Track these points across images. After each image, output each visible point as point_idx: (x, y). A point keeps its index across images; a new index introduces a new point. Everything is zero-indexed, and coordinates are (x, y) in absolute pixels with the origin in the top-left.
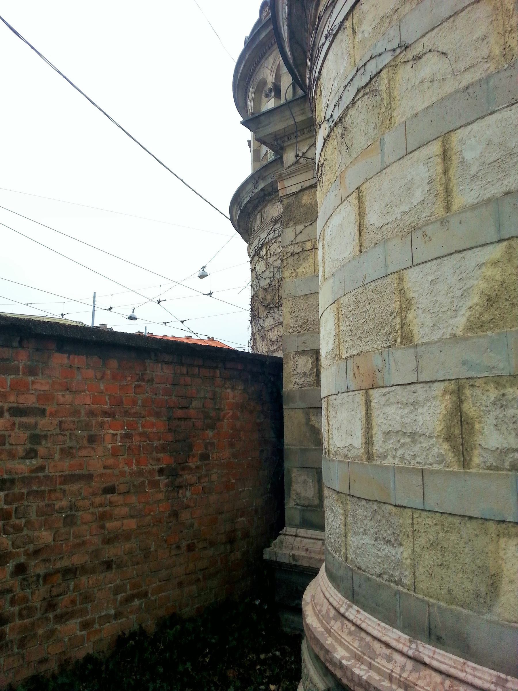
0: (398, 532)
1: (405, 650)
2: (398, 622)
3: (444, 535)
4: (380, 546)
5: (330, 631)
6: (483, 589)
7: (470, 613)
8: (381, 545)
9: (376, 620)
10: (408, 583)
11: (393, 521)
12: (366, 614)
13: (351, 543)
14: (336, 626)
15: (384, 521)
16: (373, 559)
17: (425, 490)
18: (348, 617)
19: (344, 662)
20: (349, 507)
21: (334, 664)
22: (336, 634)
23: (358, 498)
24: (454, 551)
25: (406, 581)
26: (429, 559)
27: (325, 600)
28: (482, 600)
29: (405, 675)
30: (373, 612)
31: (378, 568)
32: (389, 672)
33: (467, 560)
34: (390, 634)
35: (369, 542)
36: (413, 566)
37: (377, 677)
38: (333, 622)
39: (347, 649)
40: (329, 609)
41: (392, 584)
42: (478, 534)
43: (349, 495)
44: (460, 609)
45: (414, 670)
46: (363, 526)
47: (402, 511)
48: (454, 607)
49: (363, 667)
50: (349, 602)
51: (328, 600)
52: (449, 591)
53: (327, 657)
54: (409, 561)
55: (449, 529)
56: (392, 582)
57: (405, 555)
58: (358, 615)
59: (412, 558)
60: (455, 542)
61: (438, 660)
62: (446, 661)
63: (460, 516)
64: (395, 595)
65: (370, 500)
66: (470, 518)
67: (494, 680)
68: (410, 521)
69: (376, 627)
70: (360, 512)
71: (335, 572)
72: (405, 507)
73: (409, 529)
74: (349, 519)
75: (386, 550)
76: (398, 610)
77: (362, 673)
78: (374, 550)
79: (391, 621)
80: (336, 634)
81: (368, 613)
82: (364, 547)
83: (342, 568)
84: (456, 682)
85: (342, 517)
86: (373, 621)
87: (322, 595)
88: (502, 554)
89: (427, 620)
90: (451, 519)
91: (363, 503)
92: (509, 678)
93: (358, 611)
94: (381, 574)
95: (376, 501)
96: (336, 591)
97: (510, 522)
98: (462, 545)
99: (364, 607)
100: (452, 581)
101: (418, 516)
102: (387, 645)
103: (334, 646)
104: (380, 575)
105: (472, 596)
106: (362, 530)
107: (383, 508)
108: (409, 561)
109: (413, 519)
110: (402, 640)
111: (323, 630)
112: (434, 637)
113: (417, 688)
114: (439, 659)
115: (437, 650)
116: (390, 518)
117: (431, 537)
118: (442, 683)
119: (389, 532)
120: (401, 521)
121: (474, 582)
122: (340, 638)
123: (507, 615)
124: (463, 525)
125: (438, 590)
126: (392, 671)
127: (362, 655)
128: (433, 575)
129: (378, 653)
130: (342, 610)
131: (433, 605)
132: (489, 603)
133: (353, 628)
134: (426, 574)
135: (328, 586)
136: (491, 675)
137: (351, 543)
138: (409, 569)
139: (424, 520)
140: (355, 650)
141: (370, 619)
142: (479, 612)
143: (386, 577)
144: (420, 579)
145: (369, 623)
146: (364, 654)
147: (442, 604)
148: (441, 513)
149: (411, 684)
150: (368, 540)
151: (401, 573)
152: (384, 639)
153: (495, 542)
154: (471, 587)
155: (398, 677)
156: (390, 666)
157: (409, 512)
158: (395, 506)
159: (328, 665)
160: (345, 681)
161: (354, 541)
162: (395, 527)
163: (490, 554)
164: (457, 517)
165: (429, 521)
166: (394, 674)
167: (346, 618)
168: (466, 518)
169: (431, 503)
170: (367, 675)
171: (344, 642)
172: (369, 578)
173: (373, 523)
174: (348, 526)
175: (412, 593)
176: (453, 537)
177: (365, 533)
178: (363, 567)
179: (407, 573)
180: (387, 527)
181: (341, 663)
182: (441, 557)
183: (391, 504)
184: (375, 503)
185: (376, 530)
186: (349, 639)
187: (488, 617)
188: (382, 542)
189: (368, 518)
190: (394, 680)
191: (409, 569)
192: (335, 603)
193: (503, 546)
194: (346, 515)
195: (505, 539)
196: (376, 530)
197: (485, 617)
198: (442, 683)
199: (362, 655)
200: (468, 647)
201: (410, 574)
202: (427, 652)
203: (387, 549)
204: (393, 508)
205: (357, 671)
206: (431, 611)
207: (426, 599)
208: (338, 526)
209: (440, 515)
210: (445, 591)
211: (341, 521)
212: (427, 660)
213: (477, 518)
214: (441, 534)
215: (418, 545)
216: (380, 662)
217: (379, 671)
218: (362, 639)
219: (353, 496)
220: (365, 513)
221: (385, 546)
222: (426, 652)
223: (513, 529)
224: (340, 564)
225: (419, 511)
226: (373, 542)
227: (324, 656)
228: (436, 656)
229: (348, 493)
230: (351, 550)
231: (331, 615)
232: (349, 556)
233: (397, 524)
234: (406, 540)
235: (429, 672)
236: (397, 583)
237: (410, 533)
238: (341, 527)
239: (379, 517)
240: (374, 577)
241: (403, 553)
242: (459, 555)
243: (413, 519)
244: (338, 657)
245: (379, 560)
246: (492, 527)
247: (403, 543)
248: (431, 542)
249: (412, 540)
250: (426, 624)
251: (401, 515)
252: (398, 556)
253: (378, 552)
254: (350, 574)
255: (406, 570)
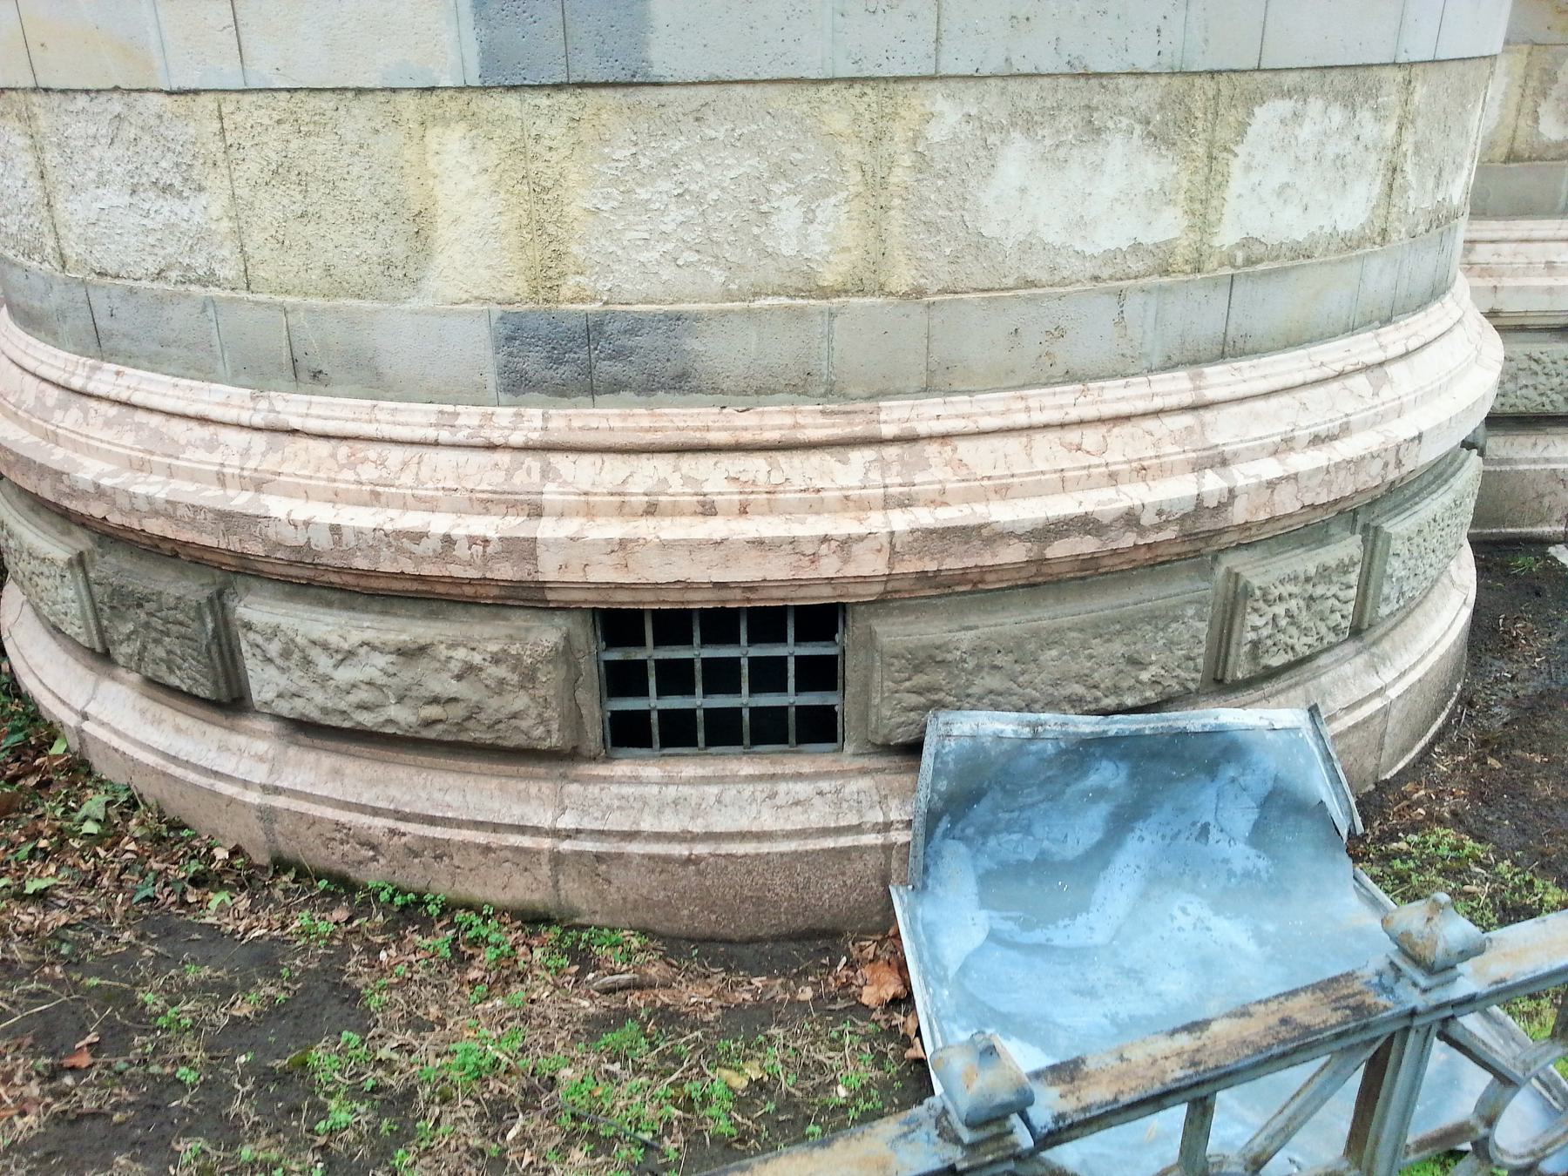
0: (188, 159)
1: (245, 418)
2: (220, 366)
3: (301, 143)
4: (146, 206)
5: (56, 435)
6: (399, 249)
7: (377, 305)
8: (150, 200)
9: (167, 378)
10: (231, 274)
11: (171, 134)
12: (140, 373)
13: (68, 217)
14: (70, 418)
15: (147, 139)
16: (133, 240)
17: (243, 38)
18: (96, 392)
19: (106, 482)
20: (43, 122)
21: (83, 495)
22: (74, 436)
23: (63, 91)
24: (329, 177)
25: (224, 272)
26: (271, 207)
27: (29, 378)
28: (399, 273)
29: (251, 464)
30: (154, 363)
31: (150, 259)
32: (216, 468)
33: (359, 194)
34: (206, 398)
35: (116, 201)
36: (238, 233)
37: (190, 487)
38: (58, 415)
39: (107, 456)
40: (43, 392)
41: (193, 288)
42: (379, 127)
43: (35, 90)
44: (356, 302)
45: (270, 448)
46: (93, 165)
47: (191, 104)
48: (341, 301)
49: (153, 478)
50: (91, 362)
51: (34, 375)
52: (327, 269)
53: (61, 487)
54: (226, 225)
55: (311, 127)
56: (191, 282)
57: (215, 211)
58: (120, 381)
59: (233, 214)
60: (328, 156)
61: (319, 417)
62: (337, 414)
63: (333, 90)
64: (204, 310)
65: (98, 91)
66: (359, 91)
67: (433, 421)
68: (216, 126)
69: (170, 393)
70: (78, 129)
71: (37, 304)
72: (196, 92)
73: (215, 146)
74: (48, 156)
75: (166, 211)
76: (216, 341)
77: (151, 490)
78: (133, 219)
79: (206, 373)
80: (74, 436)
81: (147, 369)
82: (104, 217)
83: (56, 288)
84: (359, 445)
85: (29, 158)
86: (160, 382)
87: (15, 369)
88: (432, 163)
89: (285, 343)
90: (314, 102)
91: (82, 101)
92: (460, 408)
93: (118, 373)
94: (162, 271)
95: (116, 89)
96: (50, 348)
97: (446, 88)
98: (345, 158)
99: (131, 360)
100: (331, 246)
101: (232, 108)
102: (203, 420)
103: (73, 460)
104: (159, 275)
105: (377, 269)
106: (91, 175)
107: (140, 106)
108: (226, 225)
109: (221, 118)
110: (235, 401)
111: (37, 439)
112: (307, 374)
113: (282, 478)
114: (321, 413)
115: (315, 399)
116: (162, 129)
117: (273, 155)
118: (333, 456)
119: (164, 164)
120: (191, 131)
121: (379, 236)
122: (83, 440)
123: (452, 293)
124: (342, 112)
125: (302, 274)
126: (222, 465)
127: (148, 457)
128: (287, 243)
129: (183, 442)
130: (77, 383)
131: (295, 309)
132: (412, 274)
133: (113, 411)
134: (272, 244)
135: (28, 344)
136: (426, 413)
137: (68, 217)
138: (228, 243)
139: (249, 114)
140: (128, 452)
141: (151, 381)
142: (396, 299)
143: (173, 275)
144: (258, 257)
145: (153, 388)
146: (152, 453)
147: (314, 301)
148: (288, 90)
149: (269, 477)
150: (114, 197)
151: (210, 257)
152: (191, 410)
153: (416, 140)
154: (372, 249)
155: (237, 471)
156: (217, 457)
157: (207, 101)
158: (170, 93)
159: (66, 503)
160: (115, 519)
161: (74, 210)
162: (179, 148)
163: (407, 170)
164: (328, 95)
165: (262, 116)
166: (226, 470)
167: (90, 396)
168: (350, 95)
169: (263, 72)
170: (167, 489)
171: (97, 444)
172: (131, 290)
173: (118, 150)
174: (51, 176)
175: (244, 294)
176: (324, 144)
177: (101, 182)
178: (112, 267)
179: (225, 252)
180: (159, 152)
181: (97, 486)
182: (300, 197)
183: (161, 91)
184: (116, 96)
185: (130, 167)
186: (108, 435)
187: (415, 303)
188: (151, 194)
189: (103, 141)
190: (228, 480)
191: (228, 243)
192: (54, 375)
193: (434, 146)
194: (37, 149)
195: (438, 130)
196: (130, 167)
197: (407, 306)
198: (333, 456)
199: (148, 457)
200: (379, 375)
201: (232, 253)
202: (293, 407)
203: (167, 207)
204: (168, 100)
205: (140, 490)
206: (292, 320)
207: (279, 299)
208: (20, 183)
209: (288, 95)
210: (318, 272)
211: (29, 169)
212: (296, 423)
213: (372, 90)
214: (295, 144)
215: (243, 181)
216: (195, 458)
217: (192, 476)
218: (140, 427)
219: (46, 90)
220: (92, 130)
221: (161, 202)
222: (292, 408)
223: (452, 104)
224: (49, 283)
225: (234, 96)
226: (127, 199)
227: (53, 488)
228: (313, 411)
229: (30, 84)
230: (70, 235)
231: (50, 402)
232: (67, 251)
233: (182, 139)
234: (211, 176)
235: (302, 443)
236: (203, 282)
237: (220, 156)
238: (29, 183)
239: (132, 132)
240: (145, 283)
241: (208, 208)
242: (341, 184)
243: (221, 118)
244: (89, 477)
245: (151, 240)
246: (408, 105)
247: (204, 184)
248: (274, 167)
249: (226, 172)
250: (286, 352)
251: (189, 115)
252: (197, 218)
253: (145, 221)
254: (80, 294)
255: (221, 246)
